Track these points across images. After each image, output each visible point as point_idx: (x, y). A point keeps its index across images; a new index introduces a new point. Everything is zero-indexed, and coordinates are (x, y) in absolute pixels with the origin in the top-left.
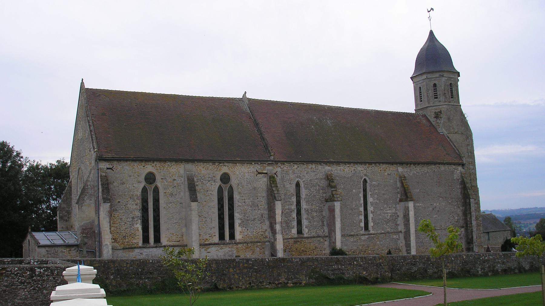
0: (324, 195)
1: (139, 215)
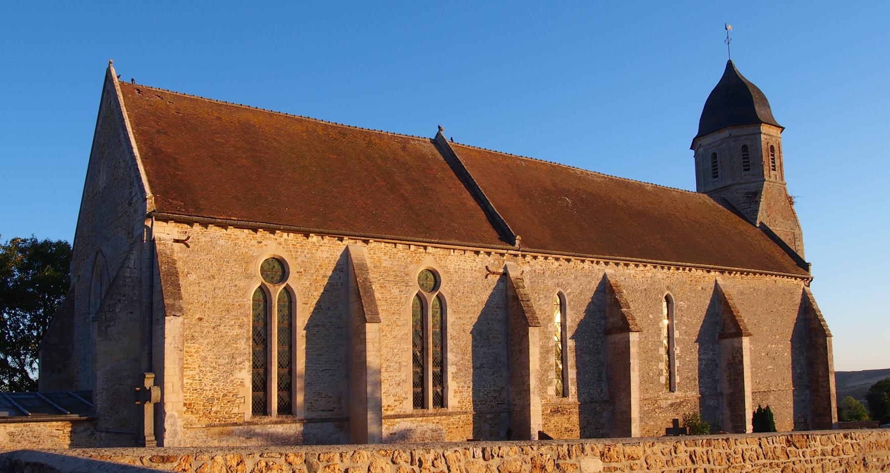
0: (603, 322)
1: (247, 351)
